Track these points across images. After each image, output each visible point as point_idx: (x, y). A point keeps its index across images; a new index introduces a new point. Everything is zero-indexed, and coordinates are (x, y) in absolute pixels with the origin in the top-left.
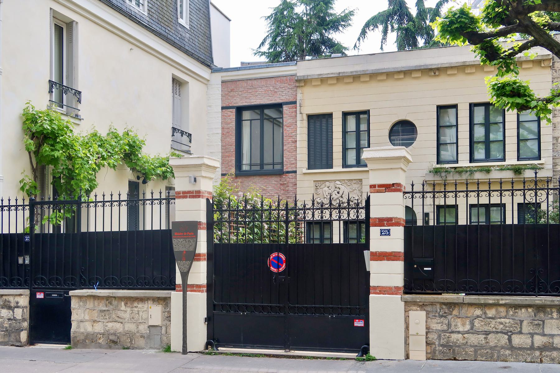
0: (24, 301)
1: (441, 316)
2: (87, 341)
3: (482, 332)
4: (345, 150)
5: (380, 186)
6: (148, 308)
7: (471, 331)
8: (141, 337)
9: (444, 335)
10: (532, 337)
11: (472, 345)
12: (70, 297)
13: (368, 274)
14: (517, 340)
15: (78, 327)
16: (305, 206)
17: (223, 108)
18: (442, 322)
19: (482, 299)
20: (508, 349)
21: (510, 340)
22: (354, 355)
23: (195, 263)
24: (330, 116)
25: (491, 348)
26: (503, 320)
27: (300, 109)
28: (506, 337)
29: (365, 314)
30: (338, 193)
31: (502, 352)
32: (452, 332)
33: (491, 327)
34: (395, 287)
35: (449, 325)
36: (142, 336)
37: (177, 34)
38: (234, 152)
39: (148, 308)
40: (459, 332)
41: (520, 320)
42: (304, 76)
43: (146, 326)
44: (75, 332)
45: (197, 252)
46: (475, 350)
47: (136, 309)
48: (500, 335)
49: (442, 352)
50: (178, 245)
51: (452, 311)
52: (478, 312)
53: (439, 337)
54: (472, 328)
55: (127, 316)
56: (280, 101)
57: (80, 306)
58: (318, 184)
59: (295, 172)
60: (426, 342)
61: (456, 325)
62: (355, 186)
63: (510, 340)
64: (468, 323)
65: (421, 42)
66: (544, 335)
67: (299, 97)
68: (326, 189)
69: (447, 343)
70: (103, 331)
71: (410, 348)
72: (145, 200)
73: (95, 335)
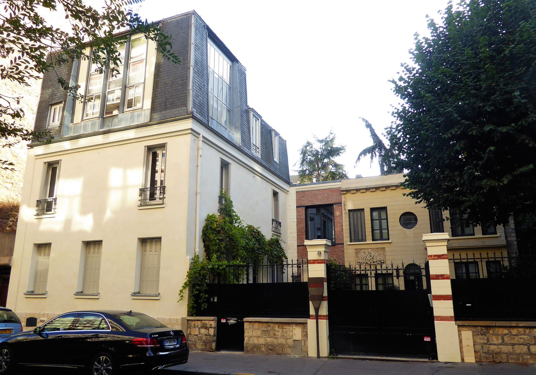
0: (214, 324)
1: (482, 335)
2: (255, 349)
3: (510, 344)
4: (373, 230)
5: (434, 256)
6: (293, 329)
8: (289, 347)
9: (486, 346)
11: (504, 352)
12: (244, 322)
13: (432, 308)
15: (249, 340)
17: (297, 207)
18: (483, 338)
20: (528, 355)
21: (529, 349)
22: (427, 360)
23: (322, 302)
24: (363, 210)
26: (522, 336)
27: (344, 207)
28: (526, 347)
29: (433, 335)
30: (371, 256)
31: (525, 356)
32: (491, 344)
33: (515, 341)
34: (450, 316)
35: (488, 340)
36: (290, 347)
37: (273, 167)
38: (305, 233)
39: (293, 329)
40: (495, 344)
41: (534, 336)
42: (346, 188)
43: (292, 341)
44: (247, 344)
45: (323, 296)
46: (507, 355)
47: (285, 330)
48: (521, 346)
49: (485, 357)
50: (312, 291)
51: (489, 331)
52: (506, 331)
53: (482, 347)
56: (332, 203)
57: (250, 327)
58: (357, 251)
59: (343, 244)
60: (475, 351)
61: (492, 340)
62: (381, 252)
63: (529, 349)
67: (343, 200)
68: (363, 254)
69: (488, 351)
70: (264, 343)
71: (464, 355)
72: (288, 265)
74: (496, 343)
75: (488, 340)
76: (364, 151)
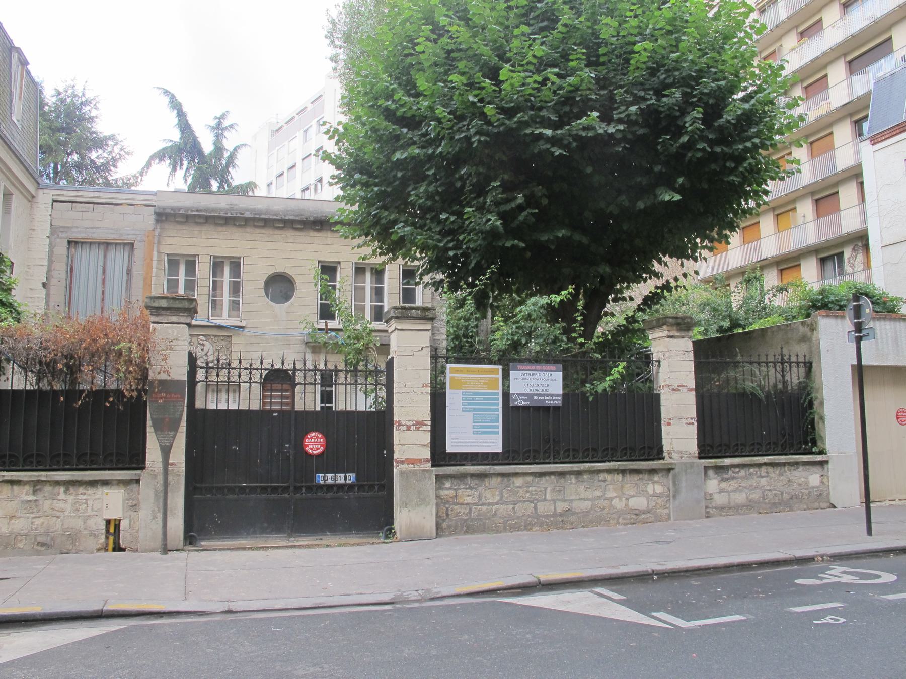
7: (501, 502)
8: (90, 536)
10: (555, 503)
14: (542, 508)
16: (336, 367)
19: (576, 467)
21: (535, 508)
25: (518, 517)
30: (202, 350)
48: (527, 503)
54: (501, 499)
55: (68, 507)
64: (497, 493)
65: (215, 185)
66: (564, 501)
73: (13, 536)
74: (491, 501)
75: (480, 497)
76: (159, 152)
